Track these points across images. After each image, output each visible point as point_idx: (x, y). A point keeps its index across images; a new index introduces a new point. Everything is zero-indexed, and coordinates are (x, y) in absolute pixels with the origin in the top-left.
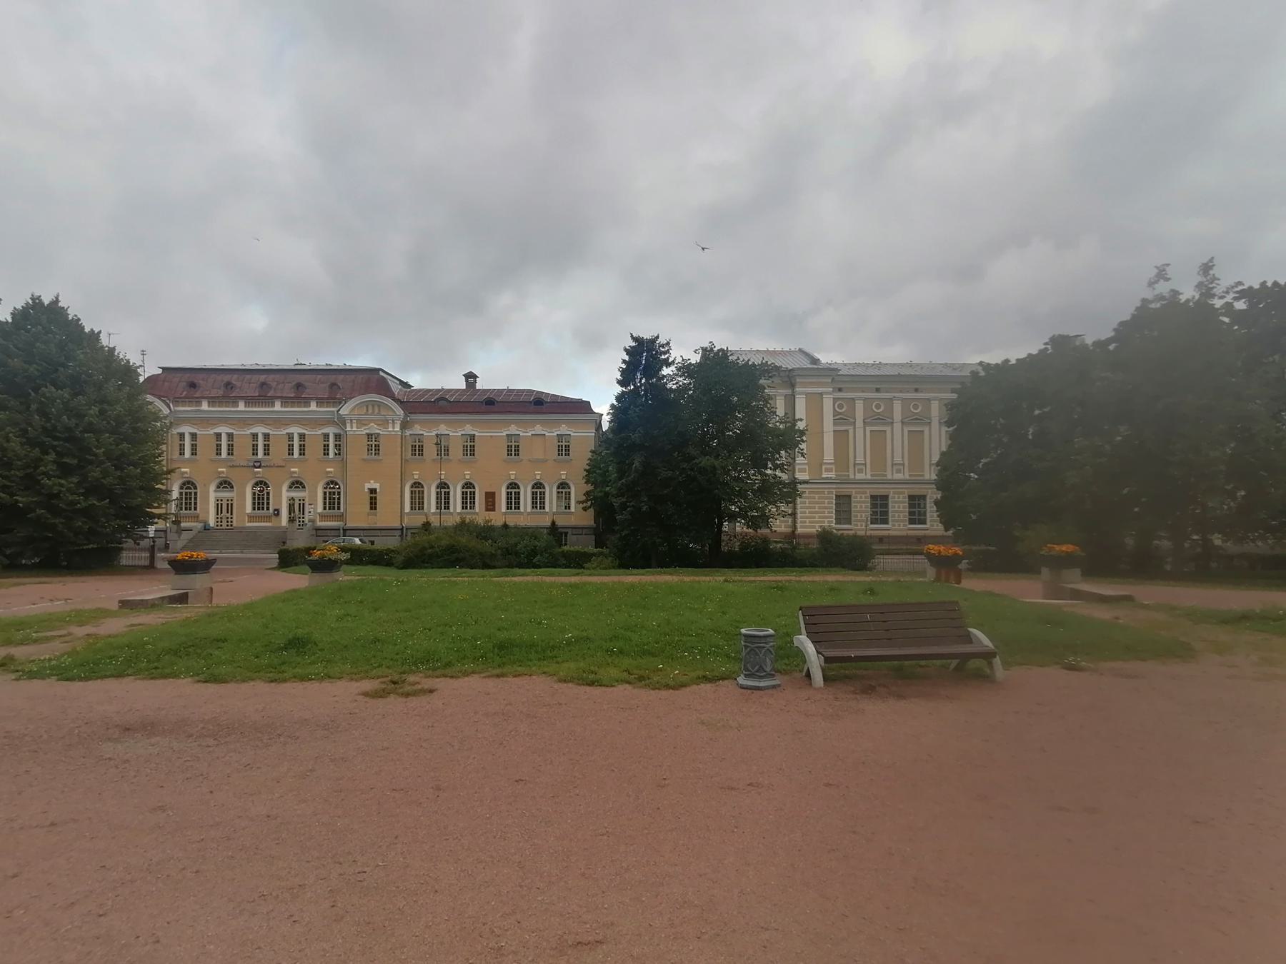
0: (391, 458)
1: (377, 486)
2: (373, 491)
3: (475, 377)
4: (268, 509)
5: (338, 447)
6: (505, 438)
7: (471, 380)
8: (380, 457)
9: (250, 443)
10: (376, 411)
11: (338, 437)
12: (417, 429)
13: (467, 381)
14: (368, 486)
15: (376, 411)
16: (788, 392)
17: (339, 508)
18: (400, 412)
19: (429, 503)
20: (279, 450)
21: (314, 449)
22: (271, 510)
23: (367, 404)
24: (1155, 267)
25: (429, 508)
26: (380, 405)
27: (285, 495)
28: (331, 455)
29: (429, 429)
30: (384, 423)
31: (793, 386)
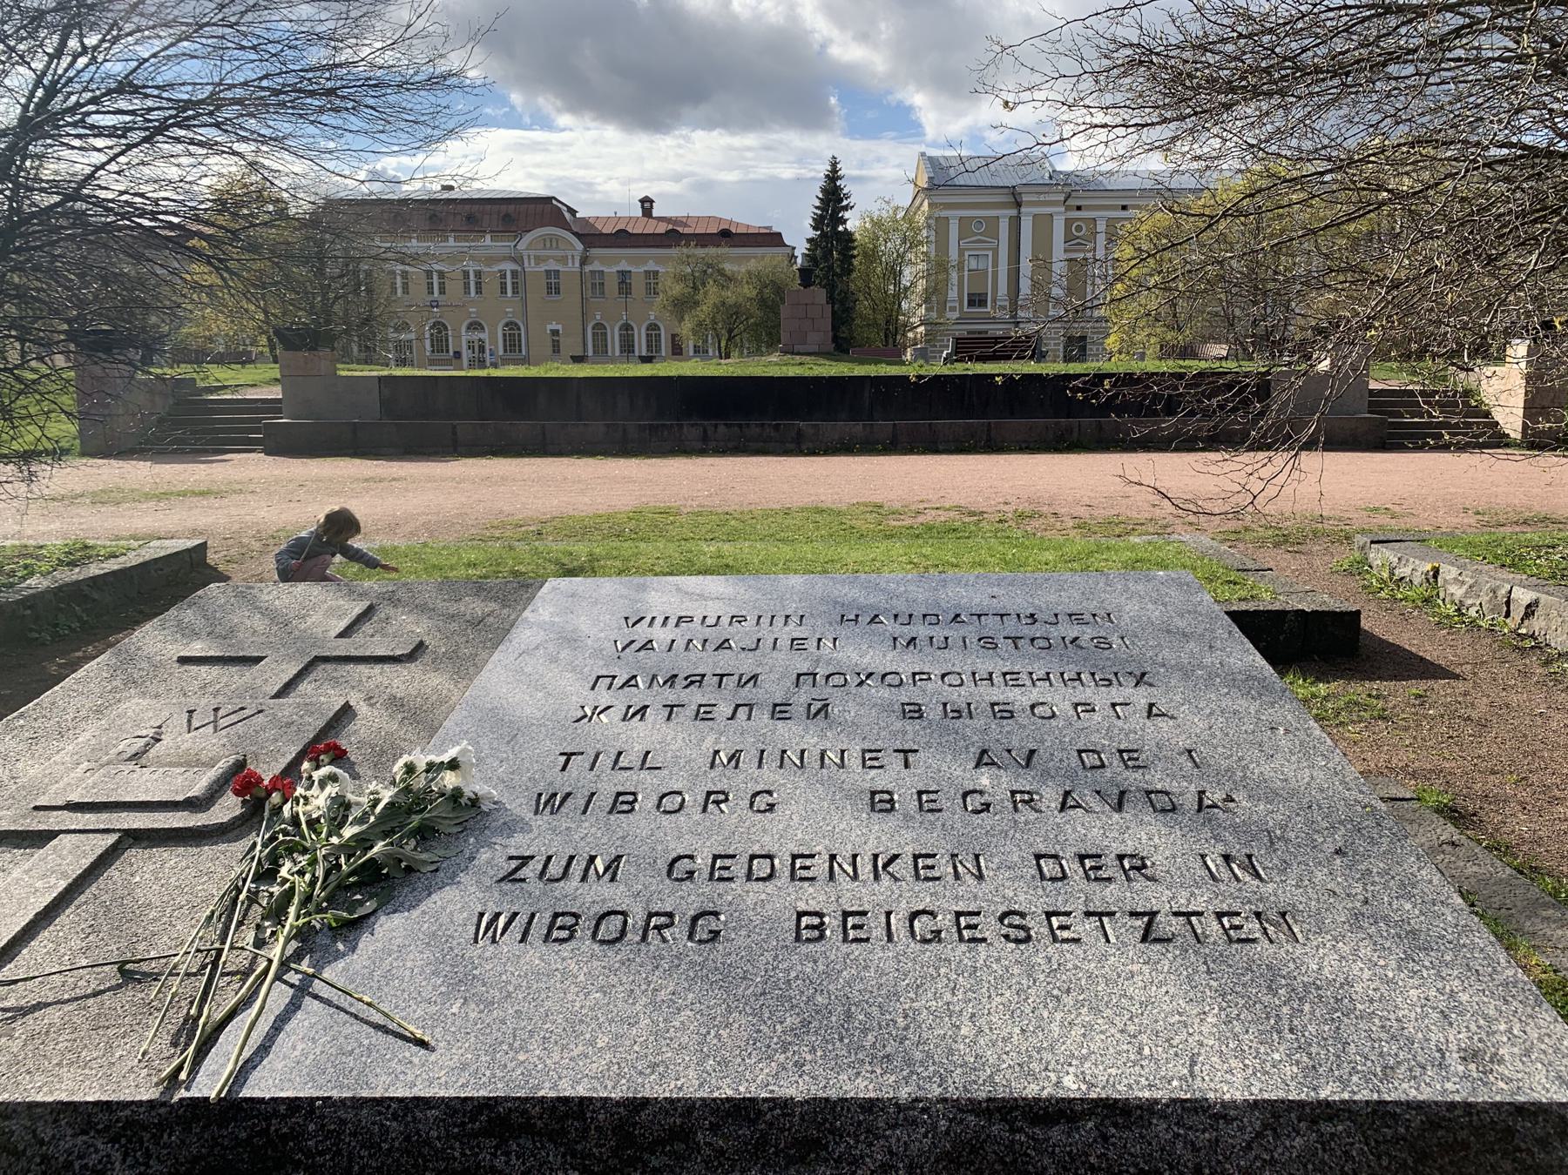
0: (570, 297)
1: (559, 327)
2: (555, 332)
3: (652, 202)
4: (448, 351)
5: (515, 286)
6: (643, 275)
7: (647, 205)
8: (562, 296)
9: (424, 281)
10: (554, 244)
11: (514, 274)
12: (596, 266)
13: (643, 207)
14: (549, 327)
15: (554, 244)
16: (1014, 212)
17: (520, 351)
18: (580, 246)
19: (613, 348)
20: (455, 288)
21: (490, 285)
22: (451, 353)
23: (544, 239)
24: (834, 164)
25: (640, 351)
26: (558, 238)
27: (465, 337)
28: (509, 293)
29: (610, 263)
30: (563, 260)
31: (1019, 205)
